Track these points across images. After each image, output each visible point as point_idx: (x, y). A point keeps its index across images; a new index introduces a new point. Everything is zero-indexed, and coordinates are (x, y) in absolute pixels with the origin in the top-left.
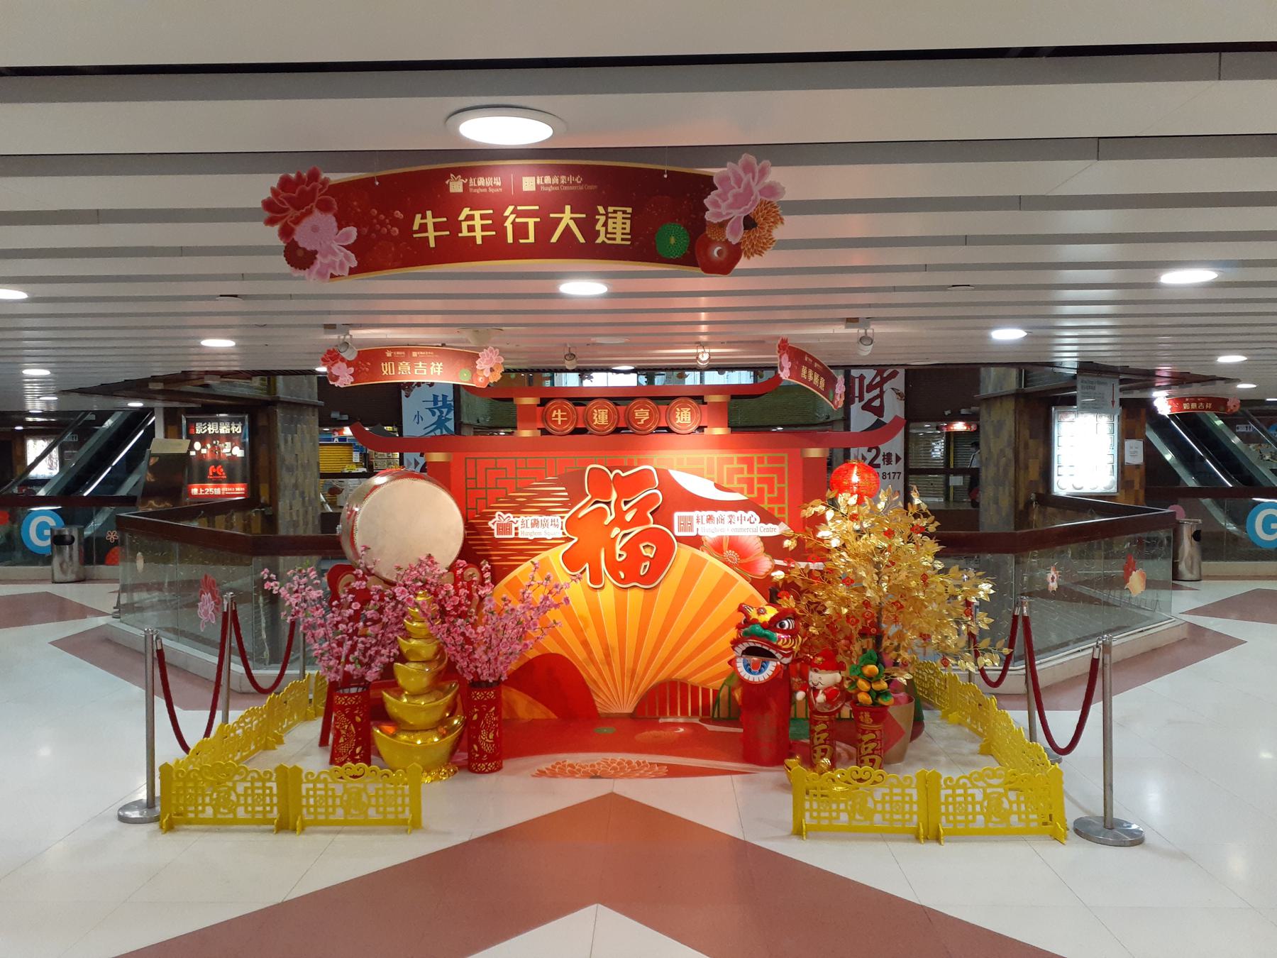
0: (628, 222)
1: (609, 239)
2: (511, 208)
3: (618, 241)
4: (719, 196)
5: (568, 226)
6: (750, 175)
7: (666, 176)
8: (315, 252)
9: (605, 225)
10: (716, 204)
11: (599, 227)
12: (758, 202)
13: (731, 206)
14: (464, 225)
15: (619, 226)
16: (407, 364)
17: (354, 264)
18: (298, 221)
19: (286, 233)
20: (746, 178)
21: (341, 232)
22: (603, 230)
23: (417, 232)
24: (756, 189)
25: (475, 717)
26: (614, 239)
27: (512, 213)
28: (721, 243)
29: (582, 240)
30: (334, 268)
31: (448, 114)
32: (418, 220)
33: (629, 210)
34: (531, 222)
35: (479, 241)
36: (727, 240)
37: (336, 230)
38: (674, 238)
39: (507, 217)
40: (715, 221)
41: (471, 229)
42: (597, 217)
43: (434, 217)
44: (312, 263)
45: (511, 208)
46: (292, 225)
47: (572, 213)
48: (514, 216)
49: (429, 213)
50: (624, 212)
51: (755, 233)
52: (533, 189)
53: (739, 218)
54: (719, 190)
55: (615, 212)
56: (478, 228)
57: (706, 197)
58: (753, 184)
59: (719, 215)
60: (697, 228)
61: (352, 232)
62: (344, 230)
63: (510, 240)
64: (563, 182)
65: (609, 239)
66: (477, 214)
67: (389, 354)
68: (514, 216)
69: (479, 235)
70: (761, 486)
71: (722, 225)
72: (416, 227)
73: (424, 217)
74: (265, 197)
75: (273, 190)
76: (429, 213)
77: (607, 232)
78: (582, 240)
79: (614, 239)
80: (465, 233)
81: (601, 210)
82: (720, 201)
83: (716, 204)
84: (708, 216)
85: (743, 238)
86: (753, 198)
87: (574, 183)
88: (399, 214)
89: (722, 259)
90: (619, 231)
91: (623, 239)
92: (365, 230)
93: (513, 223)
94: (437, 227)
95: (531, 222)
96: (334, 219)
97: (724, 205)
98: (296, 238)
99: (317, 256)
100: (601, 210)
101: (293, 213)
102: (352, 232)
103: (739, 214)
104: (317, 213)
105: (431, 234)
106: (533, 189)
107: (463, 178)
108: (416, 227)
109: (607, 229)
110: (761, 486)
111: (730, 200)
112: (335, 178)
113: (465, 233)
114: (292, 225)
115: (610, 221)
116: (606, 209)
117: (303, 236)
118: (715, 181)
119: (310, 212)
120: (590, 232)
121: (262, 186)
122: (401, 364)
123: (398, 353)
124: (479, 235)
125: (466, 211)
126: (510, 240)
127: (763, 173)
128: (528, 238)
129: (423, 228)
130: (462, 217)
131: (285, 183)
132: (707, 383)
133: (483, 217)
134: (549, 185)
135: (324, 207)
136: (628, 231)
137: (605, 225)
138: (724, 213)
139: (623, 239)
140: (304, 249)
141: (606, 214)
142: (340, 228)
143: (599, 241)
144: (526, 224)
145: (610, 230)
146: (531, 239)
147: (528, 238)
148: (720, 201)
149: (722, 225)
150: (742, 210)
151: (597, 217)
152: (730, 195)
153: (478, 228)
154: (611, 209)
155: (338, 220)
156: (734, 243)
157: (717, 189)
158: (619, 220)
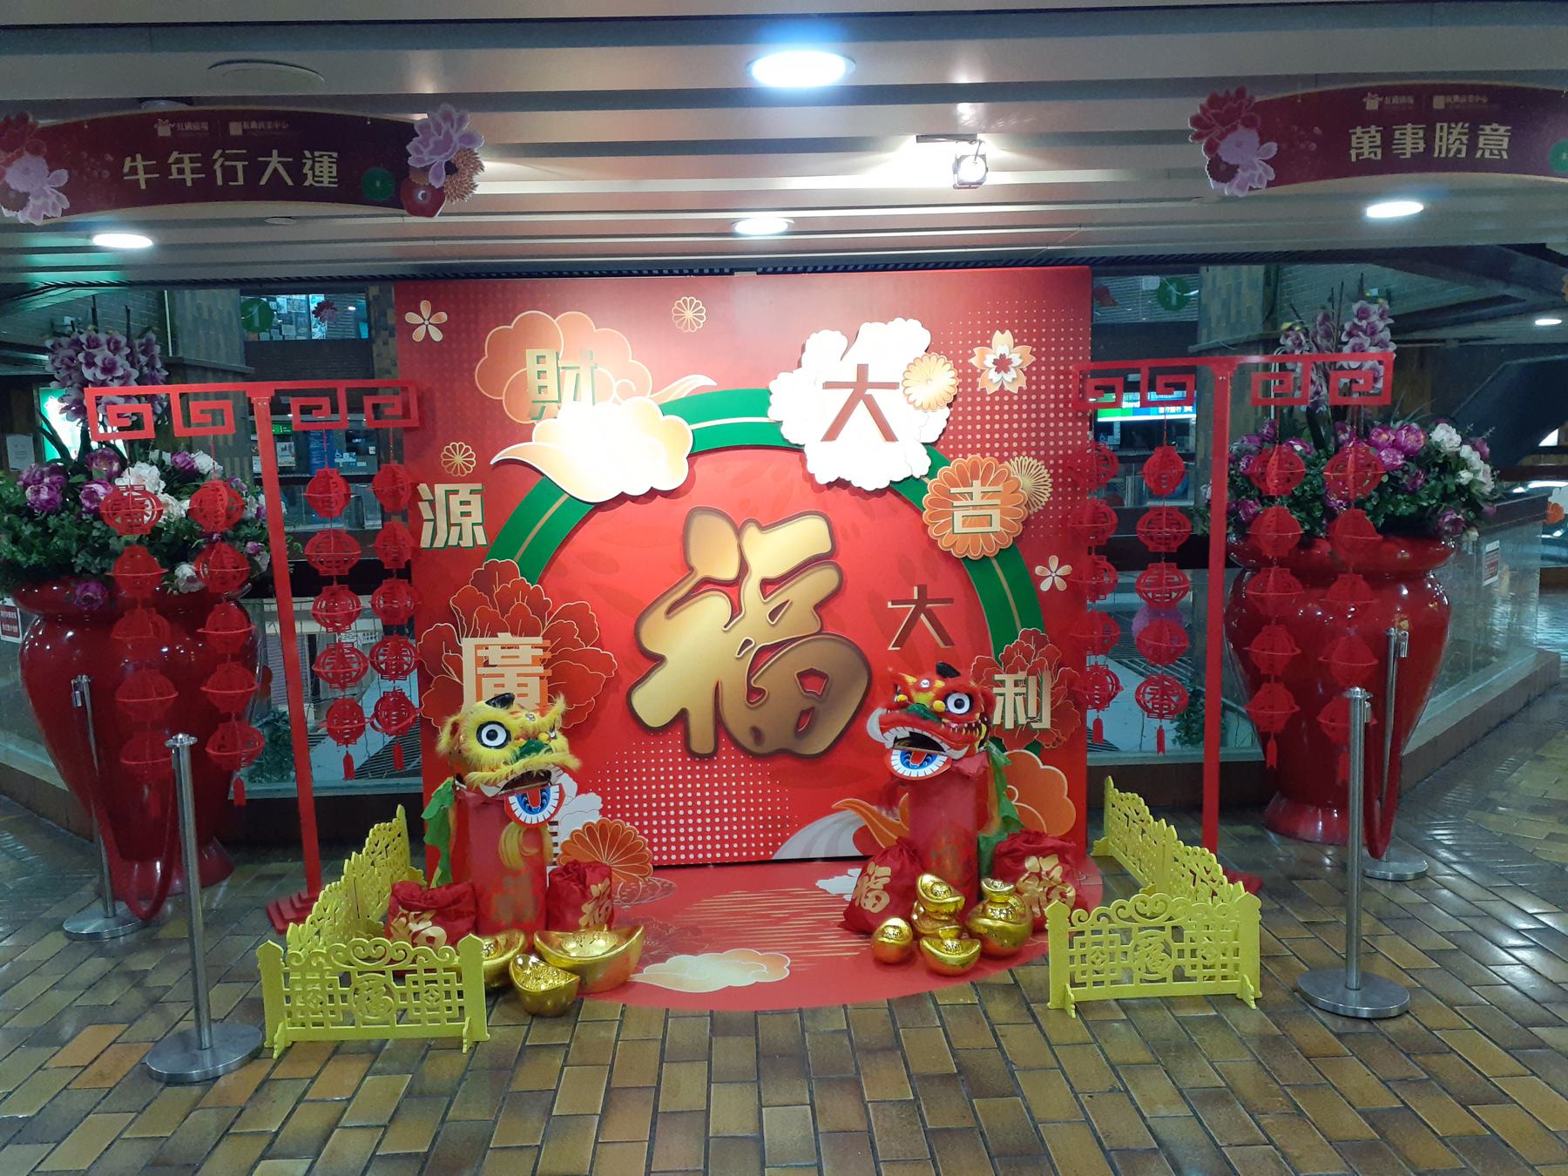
0: (334, 166)
1: (317, 182)
2: (220, 151)
3: (326, 184)
4: (421, 142)
5: (275, 170)
6: (449, 124)
7: (86, 127)
8: (27, 195)
9: (312, 168)
10: (418, 151)
11: (306, 170)
12: (458, 148)
13: (431, 153)
14: (174, 168)
15: (326, 170)
16: (1502, 129)
17: (67, 205)
18: (1223, 136)
19: (1210, 148)
20: (445, 126)
21: (52, 174)
22: (310, 174)
23: (127, 175)
24: (456, 137)
25: (922, 909)
26: (322, 182)
27: (220, 156)
28: (425, 187)
29: (290, 183)
30: (47, 211)
31: (213, 64)
32: (128, 163)
33: (335, 155)
34: (240, 165)
35: (189, 184)
36: (430, 185)
37: (1257, 145)
38: (378, 179)
39: (216, 160)
40: (418, 166)
41: (181, 171)
42: (304, 161)
43: (143, 160)
44: (1233, 177)
45: (220, 151)
46: (1217, 141)
47: (279, 156)
48: (222, 159)
49: (139, 157)
50: (330, 157)
51: (456, 179)
52: (1442, 107)
53: (440, 164)
54: (421, 136)
55: (321, 156)
56: (188, 170)
57: (407, 144)
58: (452, 132)
59: (420, 160)
60: (401, 171)
61: (1272, 148)
62: (1265, 145)
63: (220, 182)
64: (269, 127)
65: (317, 182)
66: (186, 157)
67: (1372, 104)
68: (222, 159)
69: (189, 178)
70: (1117, 430)
71: (426, 169)
72: (126, 170)
73: (134, 160)
74: (1193, 114)
75: (1202, 107)
76: (139, 157)
77: (314, 176)
78: (290, 183)
79: (322, 182)
80: (175, 175)
81: (307, 154)
82: (421, 147)
83: (418, 151)
84: (411, 162)
85: (445, 183)
86: (453, 145)
87: (1480, 102)
88: (109, 158)
89: (426, 201)
90: (326, 175)
91: (330, 182)
92: (1285, 146)
93: (222, 166)
94: (147, 170)
95: (240, 165)
96: (1256, 134)
97: (425, 151)
98: (1220, 152)
99: (1239, 170)
100: (307, 154)
101: (1218, 130)
102: (1272, 148)
103: (440, 160)
104: (1241, 128)
105: (142, 177)
106: (1442, 107)
107: (1380, 96)
108: (126, 170)
109: (314, 172)
110: (1117, 430)
111: (432, 146)
112: (44, 123)
113: (175, 175)
114: (1217, 141)
115: (317, 165)
116: (312, 154)
117: (1227, 153)
118: (416, 128)
119: (1235, 128)
120: (298, 176)
121: (1194, 105)
122: (1488, 129)
123: (189, 126)
124: (189, 178)
125: (175, 155)
126: (220, 182)
127: (462, 120)
128: (237, 181)
129: (134, 170)
130: (171, 160)
131: (1214, 101)
132: (261, 339)
133: (192, 160)
134: (253, 130)
135: (1250, 123)
136: (334, 174)
137: (312, 168)
138: (426, 159)
139: (330, 182)
140: (1226, 163)
141: (313, 158)
142: (1262, 143)
143: (307, 184)
144: (235, 167)
145: (317, 173)
146: (241, 182)
147: (237, 181)
148: (421, 147)
149: (426, 169)
150: (442, 156)
151: (304, 161)
152: (432, 141)
153: (188, 170)
154: (317, 154)
155: (1260, 135)
156: (437, 187)
157: (417, 136)
158: (326, 164)
